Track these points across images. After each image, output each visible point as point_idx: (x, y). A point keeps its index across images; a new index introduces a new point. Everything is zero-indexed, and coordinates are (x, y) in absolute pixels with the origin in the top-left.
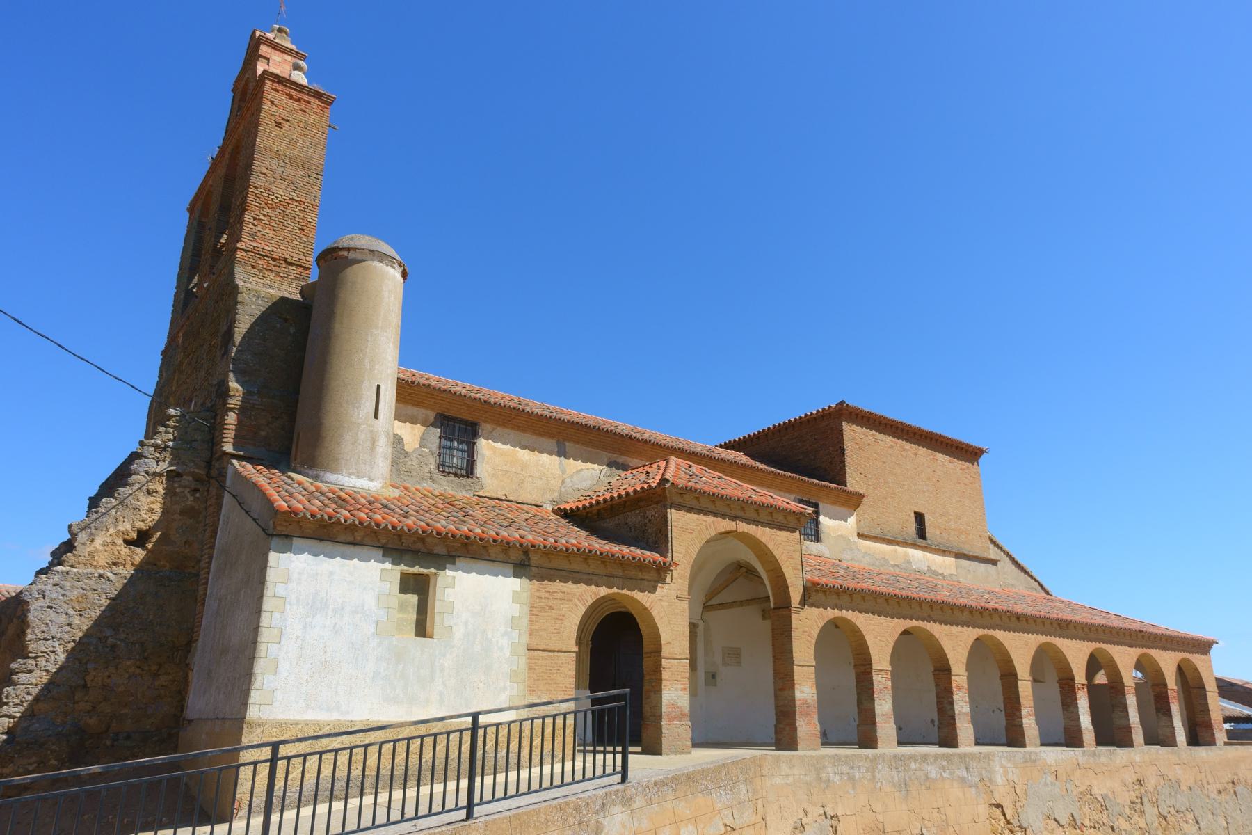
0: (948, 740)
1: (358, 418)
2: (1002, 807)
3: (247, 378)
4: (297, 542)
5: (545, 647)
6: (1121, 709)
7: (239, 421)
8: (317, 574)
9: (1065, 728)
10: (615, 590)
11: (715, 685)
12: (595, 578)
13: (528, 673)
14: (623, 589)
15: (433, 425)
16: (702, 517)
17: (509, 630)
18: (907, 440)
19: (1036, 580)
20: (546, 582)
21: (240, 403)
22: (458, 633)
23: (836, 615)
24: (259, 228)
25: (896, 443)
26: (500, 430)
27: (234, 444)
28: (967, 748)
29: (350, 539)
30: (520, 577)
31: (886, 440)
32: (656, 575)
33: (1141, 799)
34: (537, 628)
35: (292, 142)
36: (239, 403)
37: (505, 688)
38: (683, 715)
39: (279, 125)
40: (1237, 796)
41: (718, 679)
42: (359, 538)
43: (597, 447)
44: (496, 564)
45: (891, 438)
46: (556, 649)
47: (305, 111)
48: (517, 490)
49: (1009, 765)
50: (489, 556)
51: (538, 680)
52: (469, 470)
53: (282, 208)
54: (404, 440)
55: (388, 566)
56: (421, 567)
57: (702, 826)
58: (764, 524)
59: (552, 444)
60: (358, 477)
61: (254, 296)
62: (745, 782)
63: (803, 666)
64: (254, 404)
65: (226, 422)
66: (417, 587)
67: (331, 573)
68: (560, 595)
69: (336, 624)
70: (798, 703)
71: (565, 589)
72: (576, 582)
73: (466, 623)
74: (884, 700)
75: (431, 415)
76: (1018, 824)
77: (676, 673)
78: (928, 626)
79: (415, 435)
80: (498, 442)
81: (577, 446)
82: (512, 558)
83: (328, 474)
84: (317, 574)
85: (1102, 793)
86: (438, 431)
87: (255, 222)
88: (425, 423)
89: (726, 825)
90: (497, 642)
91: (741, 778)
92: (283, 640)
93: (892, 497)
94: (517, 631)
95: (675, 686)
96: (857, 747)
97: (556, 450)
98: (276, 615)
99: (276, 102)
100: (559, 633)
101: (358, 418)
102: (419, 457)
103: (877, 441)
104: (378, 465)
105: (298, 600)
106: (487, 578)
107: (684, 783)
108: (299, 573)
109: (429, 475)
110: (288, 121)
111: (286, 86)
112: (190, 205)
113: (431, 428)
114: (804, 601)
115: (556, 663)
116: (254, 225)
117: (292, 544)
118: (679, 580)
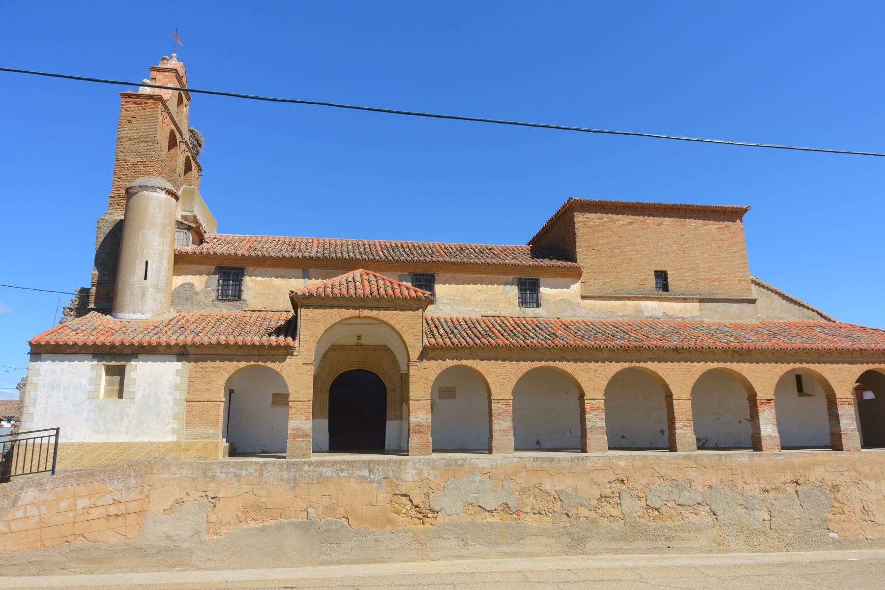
0: (836, 444)
1: (134, 281)
2: (409, 496)
3: (103, 267)
4: (44, 356)
5: (198, 400)
6: (834, 418)
7: (97, 290)
8: (55, 371)
9: (752, 436)
10: (252, 363)
12: (237, 357)
13: (186, 414)
14: (258, 362)
15: (214, 274)
16: (328, 310)
17: (173, 391)
18: (649, 215)
19: (813, 310)
20: (200, 362)
21: (96, 281)
22: (139, 395)
24: (121, 183)
25: (637, 220)
26: (260, 269)
27: (95, 303)
28: (596, 453)
29: (73, 351)
30: (182, 361)
31: (623, 220)
32: (285, 351)
33: (620, 494)
34: (194, 389)
35: (138, 129)
36: (96, 281)
37: (169, 424)
38: (306, 435)
39: (130, 122)
40: (798, 495)
42: (77, 350)
43: (333, 269)
44: (163, 355)
45: (630, 216)
46: (206, 400)
47: (144, 109)
48: (272, 303)
50: (159, 351)
51: (194, 418)
52: (238, 296)
53: (133, 168)
54: (195, 286)
55: (95, 363)
56: (106, 361)
57: (94, 500)
58: (386, 309)
59: (299, 272)
60: (134, 313)
61: (106, 222)
62: (136, 477)
63: (418, 400)
64: (105, 281)
65: (90, 292)
66: (117, 372)
67: (63, 370)
68: (210, 369)
69: (65, 395)
71: (214, 366)
72: (222, 360)
73: (144, 390)
74: (503, 420)
75: (213, 268)
76: (429, 508)
77: (301, 410)
79: (202, 281)
80: (258, 277)
81: (318, 270)
82: (174, 351)
83: (119, 314)
84: (55, 371)
85: (556, 489)
86: (217, 277)
87: (119, 180)
88: (208, 274)
89: (114, 500)
90: (165, 398)
91: (133, 474)
92: (36, 405)
93: (629, 263)
94: (179, 392)
95: (300, 418)
96: (831, 450)
97: (302, 275)
98: (32, 393)
99: (128, 109)
100: (209, 391)
101: (134, 281)
102: (205, 293)
103: (613, 221)
104: (148, 305)
105: (44, 384)
106: (159, 364)
107: (85, 477)
108: (45, 371)
109: (212, 303)
110: (135, 118)
111: (133, 98)
113: (212, 276)
115: (206, 408)
116: (118, 182)
117: (41, 357)
118: (305, 353)
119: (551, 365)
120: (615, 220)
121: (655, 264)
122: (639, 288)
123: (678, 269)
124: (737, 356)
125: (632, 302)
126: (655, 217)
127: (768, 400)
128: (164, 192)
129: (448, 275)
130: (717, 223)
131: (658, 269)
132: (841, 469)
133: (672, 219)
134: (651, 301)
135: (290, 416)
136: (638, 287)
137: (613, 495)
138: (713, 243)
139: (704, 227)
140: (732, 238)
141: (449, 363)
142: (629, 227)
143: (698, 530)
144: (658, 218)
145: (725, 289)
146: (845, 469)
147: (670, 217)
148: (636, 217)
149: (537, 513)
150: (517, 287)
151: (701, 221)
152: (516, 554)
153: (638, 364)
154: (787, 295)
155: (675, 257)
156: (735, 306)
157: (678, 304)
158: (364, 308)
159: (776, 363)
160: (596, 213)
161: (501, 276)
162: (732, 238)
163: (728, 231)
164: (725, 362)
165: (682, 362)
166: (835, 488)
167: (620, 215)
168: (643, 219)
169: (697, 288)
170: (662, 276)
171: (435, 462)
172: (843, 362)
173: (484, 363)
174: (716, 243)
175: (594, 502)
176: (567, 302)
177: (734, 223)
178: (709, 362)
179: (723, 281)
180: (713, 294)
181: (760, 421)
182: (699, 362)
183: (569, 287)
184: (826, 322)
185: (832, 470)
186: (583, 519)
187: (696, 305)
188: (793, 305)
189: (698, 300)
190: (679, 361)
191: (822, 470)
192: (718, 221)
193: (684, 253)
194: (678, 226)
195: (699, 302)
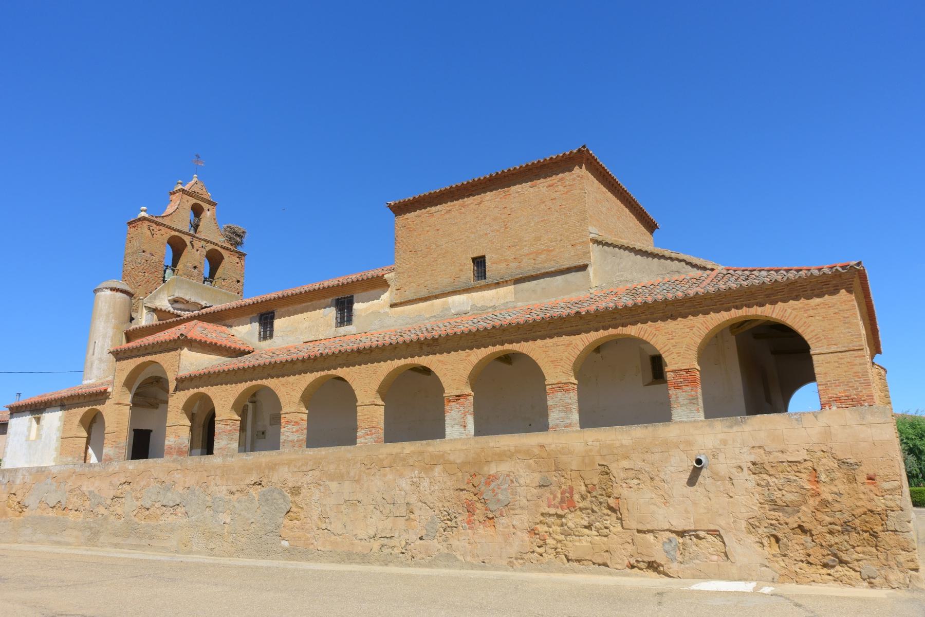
10: (91, 407)
11: (265, 438)
16: (130, 360)
18: (468, 196)
23: (195, 392)
41: (267, 434)
49: (27, 474)
70: (166, 448)
78: (265, 382)
103: (432, 215)
112: (469, 197)
114: (177, 389)
119: (259, 383)
120: (432, 213)
121: (471, 251)
122: (454, 282)
123: (499, 249)
124: (425, 347)
125: (441, 300)
126: (475, 196)
127: (457, 396)
128: (109, 290)
129: (283, 310)
130: (549, 179)
131: (475, 255)
132: (304, 468)
133: (494, 191)
134: (460, 294)
135: (105, 445)
136: (453, 281)
137: (122, 496)
138: (543, 206)
139: (532, 190)
140: (566, 193)
141: (192, 391)
142: (447, 216)
143: (172, 530)
144: (479, 196)
145: (554, 260)
146: (309, 468)
147: (491, 191)
148: (455, 202)
149: (641, 562)
150: (334, 308)
151: (529, 183)
152: (59, 543)
153: (329, 371)
154: (640, 248)
155: (495, 236)
156: (559, 279)
157: (489, 291)
158: (148, 354)
159: (471, 349)
160: (415, 211)
161: (322, 301)
162: (566, 193)
163: (562, 186)
164: (412, 356)
165: (369, 364)
166: (296, 491)
167: (439, 206)
168: (462, 203)
169: (519, 267)
170: (479, 262)
171: (32, 469)
172: (560, 335)
173: (214, 389)
174: (545, 206)
175: (109, 502)
176: (376, 314)
177: (570, 173)
178: (395, 360)
179: (552, 251)
180: (539, 270)
181: (446, 423)
182: (385, 361)
183: (378, 298)
184: (700, 272)
185: (295, 470)
186: (100, 516)
187: (511, 288)
188: (650, 259)
189: (513, 281)
190: (366, 363)
191: (286, 469)
192: (550, 177)
193: (506, 228)
194: (501, 198)
195: (514, 284)
